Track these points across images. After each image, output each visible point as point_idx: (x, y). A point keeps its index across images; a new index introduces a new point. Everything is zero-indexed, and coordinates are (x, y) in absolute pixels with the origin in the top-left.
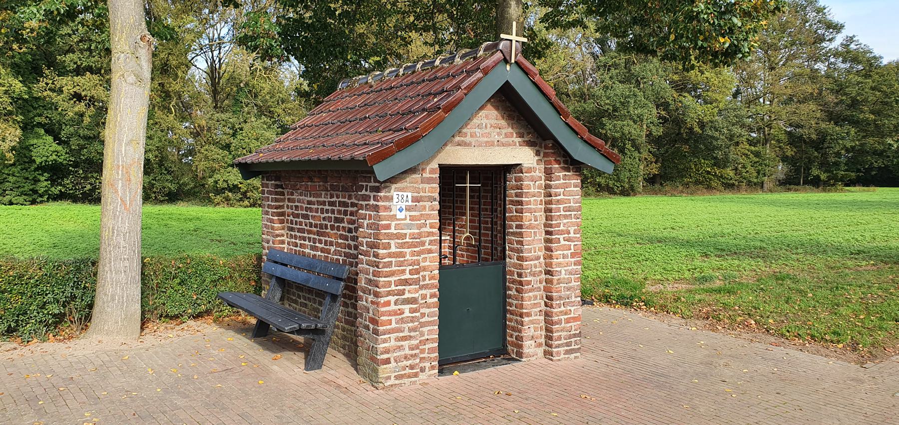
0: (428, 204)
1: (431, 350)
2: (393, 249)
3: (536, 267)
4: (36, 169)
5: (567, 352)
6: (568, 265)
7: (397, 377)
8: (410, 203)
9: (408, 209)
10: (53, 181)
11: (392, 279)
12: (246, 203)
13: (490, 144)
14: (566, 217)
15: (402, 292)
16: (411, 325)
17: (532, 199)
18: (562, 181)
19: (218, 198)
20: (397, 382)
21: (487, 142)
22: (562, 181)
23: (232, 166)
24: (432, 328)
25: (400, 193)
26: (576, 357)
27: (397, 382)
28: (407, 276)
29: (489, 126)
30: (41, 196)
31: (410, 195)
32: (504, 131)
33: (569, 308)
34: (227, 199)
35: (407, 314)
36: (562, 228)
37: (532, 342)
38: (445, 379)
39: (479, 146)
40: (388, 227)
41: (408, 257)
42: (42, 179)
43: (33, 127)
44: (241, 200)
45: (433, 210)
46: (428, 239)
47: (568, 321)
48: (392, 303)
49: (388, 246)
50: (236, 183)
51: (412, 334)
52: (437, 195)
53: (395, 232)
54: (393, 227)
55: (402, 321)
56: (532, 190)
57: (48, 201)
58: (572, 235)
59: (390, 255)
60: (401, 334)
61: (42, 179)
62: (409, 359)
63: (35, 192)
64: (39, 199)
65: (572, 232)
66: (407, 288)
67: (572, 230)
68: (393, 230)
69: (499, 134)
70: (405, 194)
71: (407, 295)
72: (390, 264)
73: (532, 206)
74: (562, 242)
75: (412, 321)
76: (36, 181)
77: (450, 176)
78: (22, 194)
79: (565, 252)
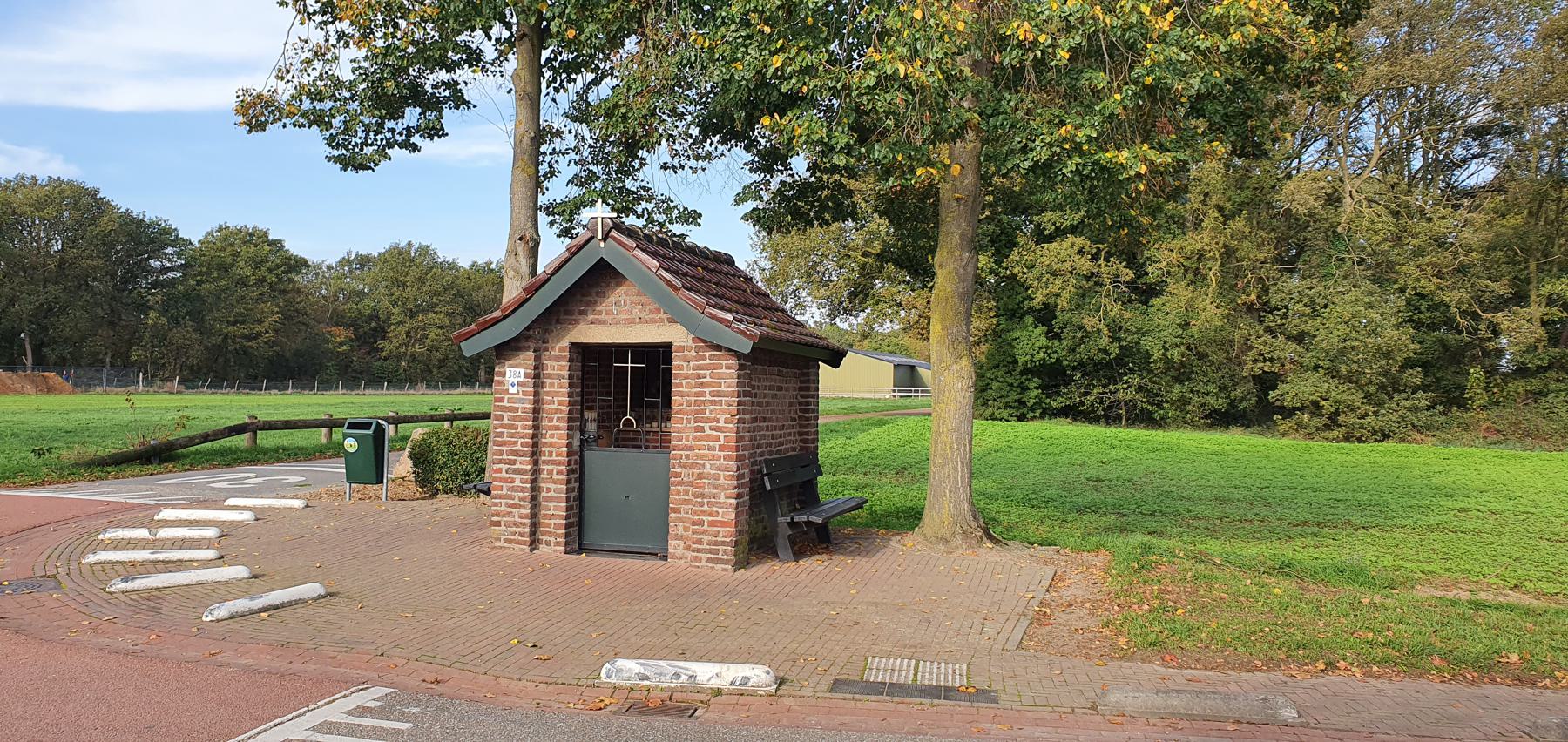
1: (557, 526)
2: (505, 421)
3: (687, 457)
4: (1022, 373)
5: (709, 560)
9: (520, 384)
10: (1049, 388)
11: (505, 449)
12: (1335, 433)
13: (631, 322)
14: (713, 403)
19: (1287, 424)
28: (519, 448)
30: (1033, 410)
34: (1300, 425)
35: (518, 483)
36: (708, 414)
42: (1032, 385)
43: (1023, 315)
44: (1327, 427)
47: (712, 524)
49: (500, 418)
50: (1313, 397)
52: (566, 373)
57: (1042, 417)
58: (722, 424)
59: (502, 426)
61: (1032, 385)
63: (1022, 403)
64: (1030, 415)
67: (722, 418)
68: (505, 404)
74: (708, 432)
76: (1024, 389)
77: (583, 353)
78: (1007, 406)
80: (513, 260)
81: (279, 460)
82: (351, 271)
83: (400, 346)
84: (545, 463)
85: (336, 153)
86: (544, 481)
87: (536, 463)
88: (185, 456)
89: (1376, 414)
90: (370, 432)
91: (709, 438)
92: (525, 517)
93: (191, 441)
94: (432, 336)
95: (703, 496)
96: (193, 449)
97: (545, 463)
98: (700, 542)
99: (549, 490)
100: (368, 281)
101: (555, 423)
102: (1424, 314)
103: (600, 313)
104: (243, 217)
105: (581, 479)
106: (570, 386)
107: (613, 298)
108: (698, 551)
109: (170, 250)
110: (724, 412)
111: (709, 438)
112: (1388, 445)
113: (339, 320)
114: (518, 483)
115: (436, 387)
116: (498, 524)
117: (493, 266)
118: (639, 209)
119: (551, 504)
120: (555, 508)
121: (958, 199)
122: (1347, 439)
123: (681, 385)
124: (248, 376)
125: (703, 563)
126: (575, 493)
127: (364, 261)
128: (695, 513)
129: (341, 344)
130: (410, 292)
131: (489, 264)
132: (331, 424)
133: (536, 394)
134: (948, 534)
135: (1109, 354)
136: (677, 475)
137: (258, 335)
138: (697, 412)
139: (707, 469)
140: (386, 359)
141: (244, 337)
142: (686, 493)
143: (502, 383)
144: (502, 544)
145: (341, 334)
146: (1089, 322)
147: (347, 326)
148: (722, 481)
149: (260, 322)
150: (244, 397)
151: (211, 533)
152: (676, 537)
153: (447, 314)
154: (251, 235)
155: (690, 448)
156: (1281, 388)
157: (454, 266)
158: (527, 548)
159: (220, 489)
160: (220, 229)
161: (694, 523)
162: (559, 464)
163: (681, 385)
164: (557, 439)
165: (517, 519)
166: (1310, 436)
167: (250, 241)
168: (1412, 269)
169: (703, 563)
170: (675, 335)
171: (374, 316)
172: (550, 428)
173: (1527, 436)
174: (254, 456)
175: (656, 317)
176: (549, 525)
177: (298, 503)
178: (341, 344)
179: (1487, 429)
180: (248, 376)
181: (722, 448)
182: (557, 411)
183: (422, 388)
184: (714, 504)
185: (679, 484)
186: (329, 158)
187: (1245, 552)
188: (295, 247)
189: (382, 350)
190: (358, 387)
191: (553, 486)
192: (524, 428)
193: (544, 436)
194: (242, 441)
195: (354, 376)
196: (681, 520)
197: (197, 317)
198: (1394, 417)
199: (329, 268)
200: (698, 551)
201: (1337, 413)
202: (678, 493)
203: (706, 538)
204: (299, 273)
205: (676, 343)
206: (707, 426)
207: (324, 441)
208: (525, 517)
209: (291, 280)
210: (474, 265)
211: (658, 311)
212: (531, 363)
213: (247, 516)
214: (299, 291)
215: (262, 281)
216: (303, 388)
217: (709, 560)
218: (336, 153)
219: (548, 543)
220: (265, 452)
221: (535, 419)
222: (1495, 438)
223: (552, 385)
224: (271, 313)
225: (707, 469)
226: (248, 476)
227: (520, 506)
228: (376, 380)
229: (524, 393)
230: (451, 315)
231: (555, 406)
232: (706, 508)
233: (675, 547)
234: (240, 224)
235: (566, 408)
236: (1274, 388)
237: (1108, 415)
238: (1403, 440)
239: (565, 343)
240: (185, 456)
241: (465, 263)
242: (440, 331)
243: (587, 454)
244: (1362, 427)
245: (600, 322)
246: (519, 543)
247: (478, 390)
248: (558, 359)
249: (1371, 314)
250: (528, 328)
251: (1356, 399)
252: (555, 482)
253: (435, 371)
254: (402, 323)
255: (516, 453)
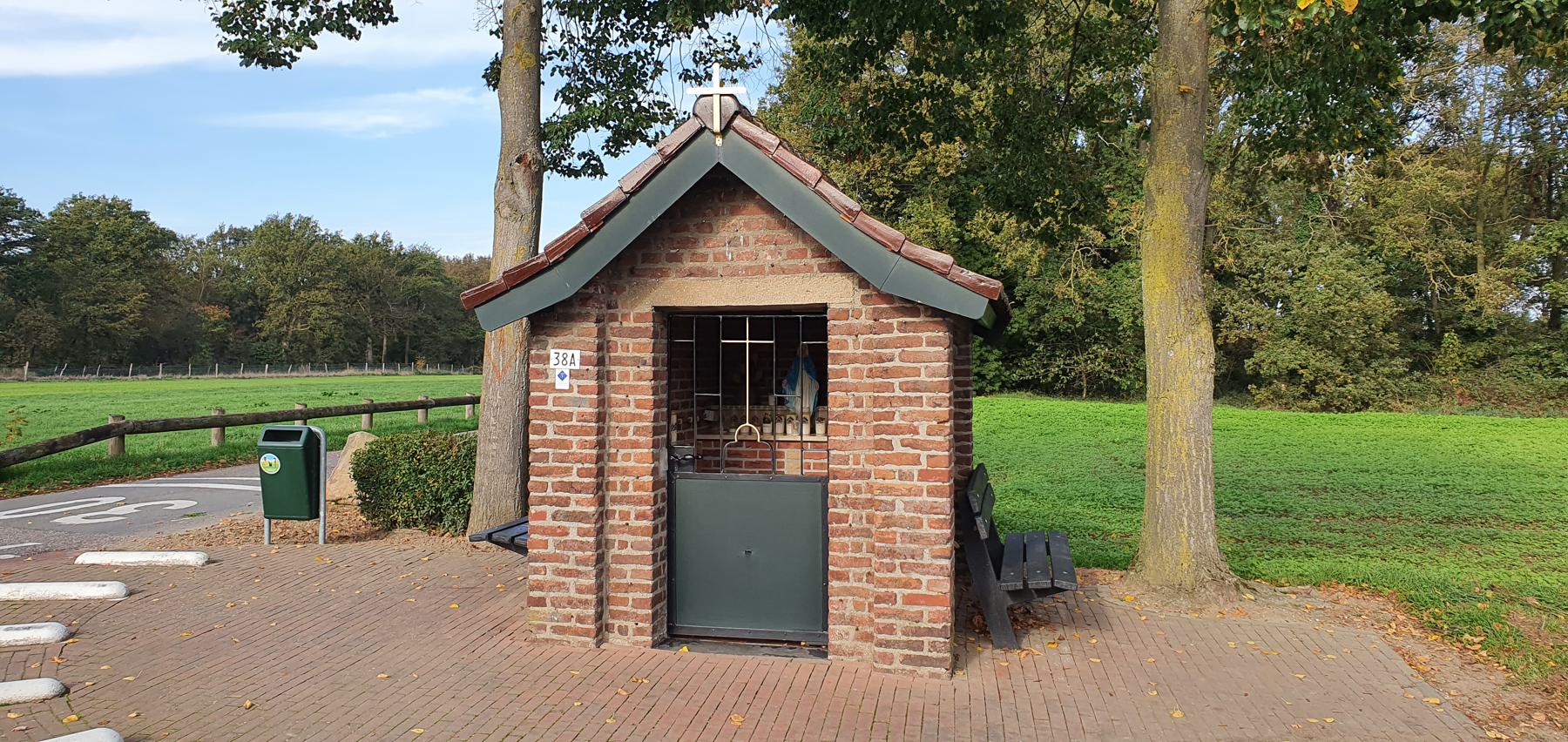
0: (632, 370)
1: (638, 603)
2: (550, 435)
3: (858, 489)
6: (910, 492)
7: (555, 630)
8: (577, 367)
9: (574, 375)
10: (1008, 361)
11: (549, 480)
12: (1314, 403)
14: (906, 401)
15: (566, 502)
16: (579, 553)
17: (849, 367)
18: (896, 334)
19: (1263, 393)
20: (555, 636)
21: (747, 268)
22: (896, 334)
23: (1491, 332)
24: (639, 567)
25: (561, 351)
26: (933, 675)
27: (555, 636)
28: (574, 478)
29: (752, 240)
30: (992, 383)
31: (577, 353)
32: (785, 249)
33: (914, 576)
34: (1278, 395)
35: (573, 536)
36: (897, 420)
37: (851, 629)
38: (664, 653)
39: (732, 275)
40: (543, 401)
41: (575, 449)
42: (992, 358)
44: (1305, 397)
45: (640, 379)
46: (632, 425)
47: (909, 600)
48: (549, 516)
49: (543, 430)
50: (1292, 366)
51: (581, 568)
52: (648, 356)
53: (554, 409)
54: (550, 402)
55: (565, 545)
56: (850, 350)
57: (1001, 391)
58: (922, 436)
59: (544, 444)
60: (563, 566)
61: (992, 358)
62: (576, 606)
64: (989, 388)
65: (923, 429)
66: (574, 496)
67: (923, 427)
68: (550, 407)
69: (772, 253)
70: (570, 353)
71: (573, 507)
72: (545, 457)
73: (850, 380)
74: (898, 449)
75: (580, 549)
77: (672, 321)
79: (905, 468)
80: (507, 191)
81: (156, 473)
82: (224, 246)
83: (281, 325)
84: (614, 500)
85: (232, 37)
86: (614, 530)
87: (601, 502)
88: (21, 474)
89: (1355, 381)
90: (299, 444)
91: (900, 459)
92: (588, 590)
93: (30, 453)
94: (315, 314)
95: (892, 553)
96: (35, 463)
97: (614, 500)
98: (890, 629)
99: (623, 545)
100: (244, 256)
101: (631, 436)
102: (1405, 280)
103: (704, 257)
104: (102, 183)
105: (670, 525)
106: (656, 376)
107: (724, 234)
108: (887, 644)
109: (15, 222)
110: (926, 416)
111: (900, 459)
112: (1370, 415)
113: (212, 298)
114: (573, 536)
115: (321, 369)
116: (540, 602)
117: (379, 239)
118: (651, 133)
119: (628, 568)
120: (636, 574)
121: (1183, 94)
122: (1326, 408)
123: (844, 373)
124: (111, 361)
125: (897, 665)
126: (663, 548)
127: (239, 235)
128: (881, 583)
129: (216, 324)
130: (290, 267)
131: (374, 237)
132: (223, 422)
133: (601, 390)
134: (1188, 581)
135: (1075, 323)
136: (842, 518)
137: (122, 315)
138: (878, 417)
139: (899, 510)
140: (265, 339)
141: (106, 317)
142: (858, 548)
143: (543, 374)
144: (548, 634)
145: (216, 313)
146: (1060, 288)
147: (221, 304)
148: (926, 530)
149: (123, 301)
150: (107, 384)
151: (47, 633)
152: (842, 620)
153: (331, 291)
154: (110, 206)
155: (865, 475)
156: (1259, 355)
157: (337, 239)
158: (591, 641)
159: (72, 529)
160: (74, 200)
161: (879, 599)
162: (640, 501)
163: (844, 373)
164: (636, 462)
165: (573, 594)
166: (1287, 406)
167: (110, 213)
168: (1388, 229)
169: (897, 665)
170: (835, 292)
171: (251, 294)
172: (623, 445)
173: (1501, 401)
174: (123, 469)
175: (800, 263)
176: (624, 602)
177: (193, 558)
178: (216, 324)
179: (1461, 395)
180: (111, 361)
181: (924, 475)
182: (633, 417)
183: (306, 371)
184: (912, 567)
185: (844, 533)
186: (223, 46)
187: (1433, 573)
188: (162, 219)
189: (261, 330)
190: (236, 370)
191: (630, 538)
192: (581, 446)
193: (613, 457)
194: (107, 446)
195: (233, 355)
196: (849, 591)
197: (51, 297)
198: (1372, 384)
199: (200, 243)
200: (887, 644)
201: (1315, 382)
202: (844, 548)
203: (900, 624)
204: (167, 247)
205: (834, 306)
206: (896, 440)
207: (214, 443)
208: (588, 590)
209: (158, 256)
210: (358, 238)
211: (803, 253)
212: (593, 340)
213: (111, 590)
214: (167, 267)
215: (124, 257)
216: (175, 372)
217: (907, 660)
218: (232, 37)
219: (623, 631)
220: (136, 461)
221: (600, 431)
222: (1473, 404)
223: (626, 376)
224: (136, 293)
225: (899, 510)
226: (112, 503)
227: (578, 574)
228: (255, 362)
229: (582, 389)
230: (333, 291)
231: (632, 409)
232: (898, 574)
233: (839, 634)
234: (98, 194)
235: (648, 413)
236: (1251, 355)
237: (1071, 391)
238: (1382, 408)
239: (646, 307)
240: (21, 474)
241: (348, 237)
242: (323, 309)
243: (680, 484)
244: (1342, 395)
245: (704, 273)
246: (577, 633)
247: (367, 370)
248: (634, 333)
249: (1353, 276)
250: (586, 287)
251: (1334, 366)
252: (633, 532)
253: (319, 352)
254: (282, 300)
255: (570, 487)
